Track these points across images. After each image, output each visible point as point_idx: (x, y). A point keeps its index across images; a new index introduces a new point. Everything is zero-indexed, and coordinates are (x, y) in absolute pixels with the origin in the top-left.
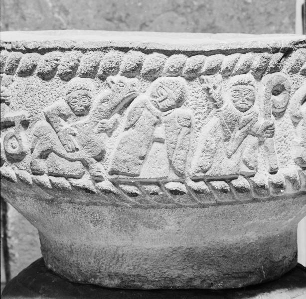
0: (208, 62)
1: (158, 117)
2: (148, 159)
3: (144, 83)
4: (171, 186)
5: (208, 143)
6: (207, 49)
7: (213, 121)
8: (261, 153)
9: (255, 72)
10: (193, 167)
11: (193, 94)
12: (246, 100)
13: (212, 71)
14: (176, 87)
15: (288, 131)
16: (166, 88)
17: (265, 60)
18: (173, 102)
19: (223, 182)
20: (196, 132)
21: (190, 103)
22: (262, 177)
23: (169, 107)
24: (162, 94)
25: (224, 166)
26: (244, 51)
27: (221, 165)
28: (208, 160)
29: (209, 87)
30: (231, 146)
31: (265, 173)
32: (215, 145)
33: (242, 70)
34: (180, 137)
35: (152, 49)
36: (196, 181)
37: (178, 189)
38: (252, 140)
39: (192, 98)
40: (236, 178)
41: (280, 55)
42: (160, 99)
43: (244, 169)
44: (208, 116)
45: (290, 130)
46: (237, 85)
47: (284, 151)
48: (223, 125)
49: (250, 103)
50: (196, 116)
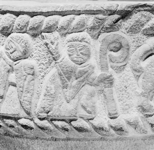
0: (47, 21)
1: (10, 66)
2: (6, 98)
3: (2, 38)
4: (23, 121)
5: (48, 89)
6: (44, 10)
7: (53, 71)
8: (101, 100)
9: (90, 31)
10: (38, 107)
11: (36, 48)
12: (81, 55)
13: (49, 30)
14: (21, 42)
15: (129, 82)
16: (15, 42)
17: (99, 21)
18: (20, 54)
19: (64, 122)
20: (40, 79)
21: (34, 55)
22: (102, 120)
23: (17, 58)
24: (12, 47)
25: (63, 108)
26: (79, 13)
27: (61, 108)
28: (49, 103)
29: (48, 42)
30: (69, 92)
31: (104, 117)
32: (54, 91)
33: (76, 28)
34: (26, 83)
35: (5, 10)
36: (41, 119)
37: (27, 125)
38: (88, 88)
39: (35, 52)
40: (75, 120)
41: (116, 16)
42: (11, 51)
43: (82, 112)
44: (50, 66)
45: (131, 82)
46: (72, 41)
47: (125, 99)
48: (60, 75)
49: (85, 57)
50: (40, 66)
